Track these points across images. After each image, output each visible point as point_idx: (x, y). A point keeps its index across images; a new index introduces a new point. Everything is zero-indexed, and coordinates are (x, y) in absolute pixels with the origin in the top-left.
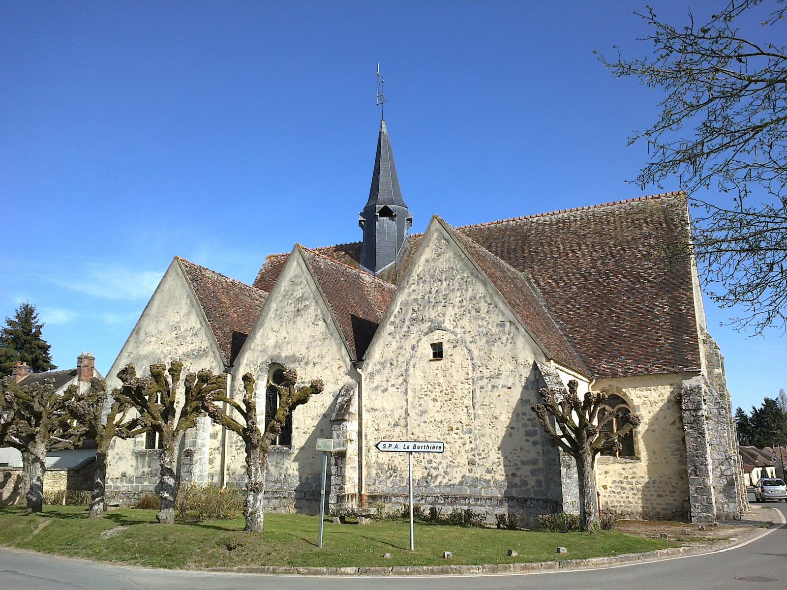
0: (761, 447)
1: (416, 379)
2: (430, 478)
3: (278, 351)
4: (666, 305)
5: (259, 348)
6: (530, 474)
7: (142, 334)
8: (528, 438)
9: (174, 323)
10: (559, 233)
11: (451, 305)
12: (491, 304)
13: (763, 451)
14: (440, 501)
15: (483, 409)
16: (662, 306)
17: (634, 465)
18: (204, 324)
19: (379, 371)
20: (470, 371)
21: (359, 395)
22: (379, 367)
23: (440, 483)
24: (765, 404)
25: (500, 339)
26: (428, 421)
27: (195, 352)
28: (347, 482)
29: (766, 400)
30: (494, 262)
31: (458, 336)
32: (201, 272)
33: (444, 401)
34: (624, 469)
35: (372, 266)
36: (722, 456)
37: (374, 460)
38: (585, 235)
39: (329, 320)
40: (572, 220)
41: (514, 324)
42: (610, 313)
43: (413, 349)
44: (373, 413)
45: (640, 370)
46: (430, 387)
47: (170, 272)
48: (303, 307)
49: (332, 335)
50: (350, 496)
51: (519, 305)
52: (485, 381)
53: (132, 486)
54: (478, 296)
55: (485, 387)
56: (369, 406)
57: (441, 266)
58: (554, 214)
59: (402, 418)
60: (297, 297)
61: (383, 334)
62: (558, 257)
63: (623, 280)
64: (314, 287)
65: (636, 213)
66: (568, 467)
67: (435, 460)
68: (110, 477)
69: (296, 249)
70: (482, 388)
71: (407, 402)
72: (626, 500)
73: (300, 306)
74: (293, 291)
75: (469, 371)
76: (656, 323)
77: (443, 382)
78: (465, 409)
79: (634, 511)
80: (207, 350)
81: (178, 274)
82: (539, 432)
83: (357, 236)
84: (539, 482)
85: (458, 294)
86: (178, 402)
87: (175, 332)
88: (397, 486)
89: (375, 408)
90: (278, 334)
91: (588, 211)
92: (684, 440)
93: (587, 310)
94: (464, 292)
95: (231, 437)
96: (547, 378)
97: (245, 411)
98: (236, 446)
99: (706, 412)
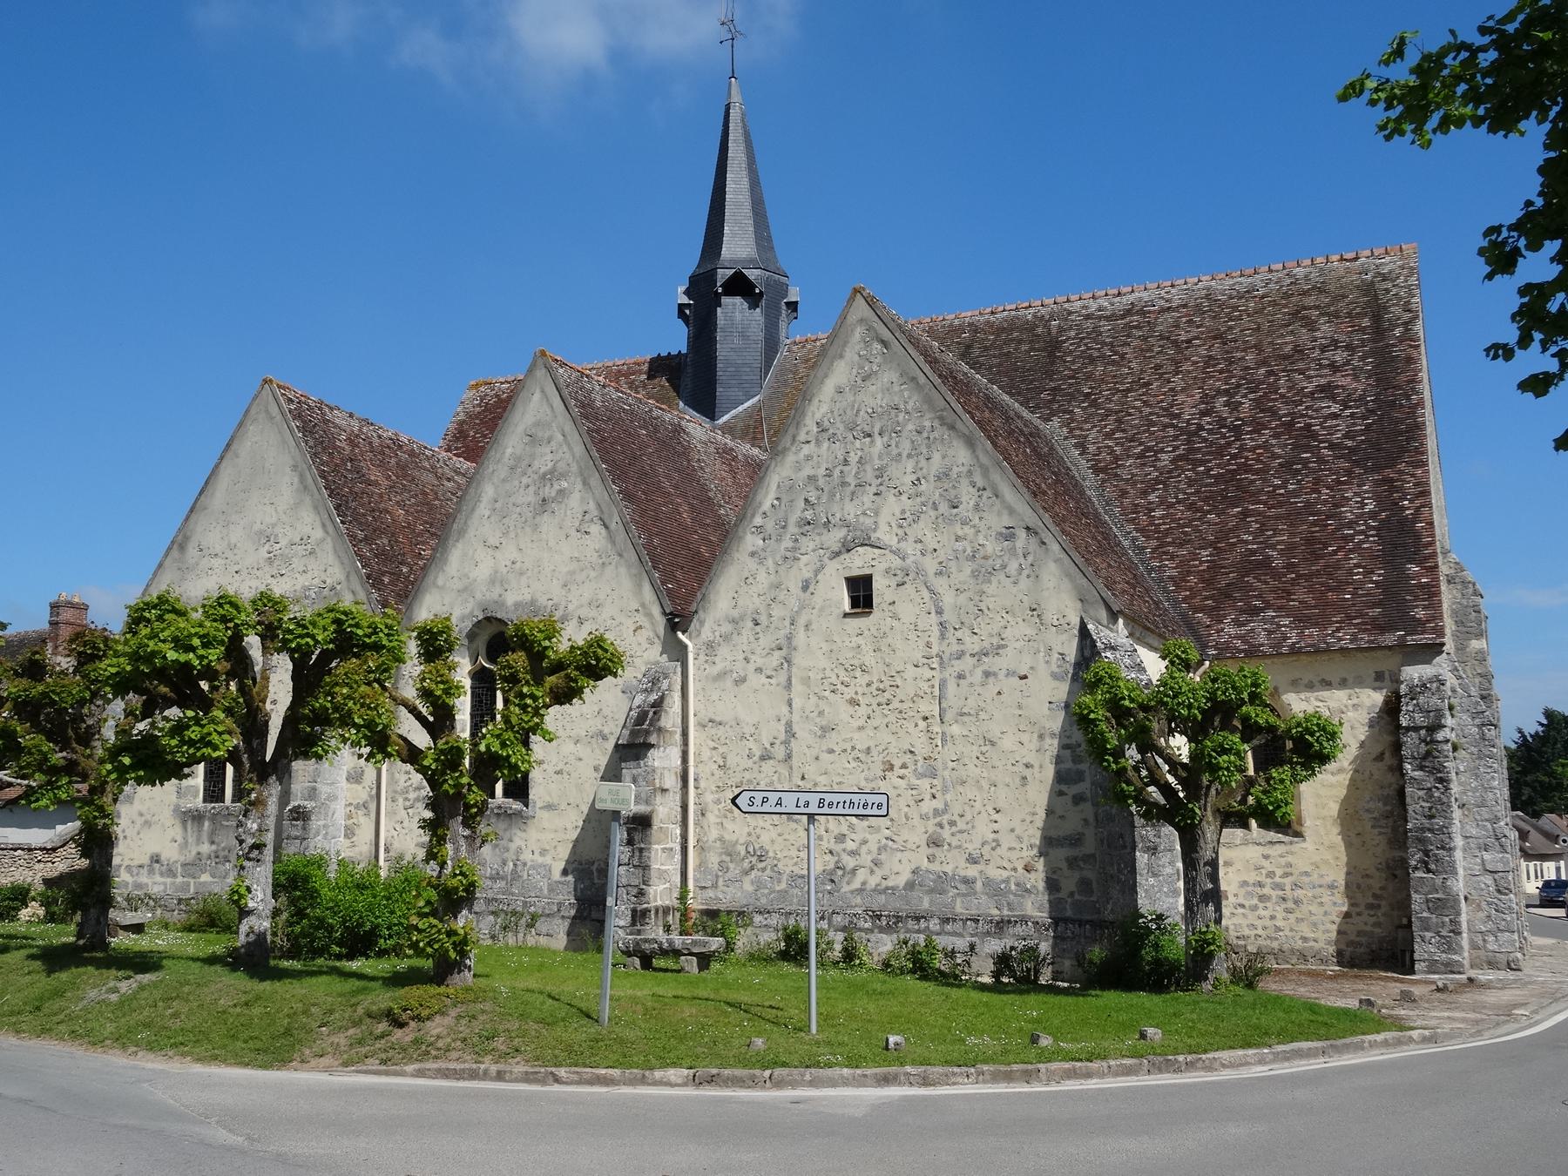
0: (1536, 815)
1: (812, 657)
2: (840, 872)
3: (497, 590)
4: (1368, 498)
5: (457, 585)
6: (1064, 865)
7: (192, 551)
8: (1064, 788)
9: (263, 527)
10: (1130, 337)
11: (893, 491)
12: (984, 489)
13: (1540, 822)
14: (861, 924)
15: (964, 723)
16: (1361, 501)
17: (1288, 847)
18: (330, 529)
19: (726, 638)
20: (934, 640)
21: (682, 689)
22: (727, 628)
23: (864, 883)
24: (1545, 722)
25: (1004, 567)
26: (838, 749)
27: (312, 592)
28: (654, 880)
29: (1549, 714)
30: (988, 397)
31: (909, 561)
32: (324, 414)
33: (875, 706)
34: (1266, 857)
35: (706, 405)
36: (1487, 831)
37: (714, 834)
38: (1189, 341)
39: (615, 521)
40: (1161, 307)
41: (1036, 533)
42: (1245, 514)
43: (805, 588)
44: (713, 731)
45: (1309, 641)
46: (842, 673)
47: (253, 411)
48: (553, 494)
49: (620, 555)
50: (660, 912)
51: (1045, 493)
52: (969, 661)
53: (173, 883)
54: (956, 470)
55: (968, 675)
56: (705, 715)
57: (872, 403)
58: (1119, 294)
59: (778, 742)
60: (542, 471)
61: (736, 555)
62: (1129, 390)
63: (1274, 442)
64: (579, 449)
65: (1305, 293)
66: (1153, 850)
67: (853, 836)
68: (126, 863)
69: (540, 362)
70: (960, 676)
71: (790, 705)
72: (1268, 923)
73: (549, 492)
74: (533, 456)
75: (931, 639)
76: (1347, 539)
77: (873, 662)
78: (922, 724)
79: (1286, 947)
80: (338, 587)
81: (272, 418)
82: (1087, 774)
83: (676, 340)
84: (1085, 885)
85: (910, 465)
86: (274, 702)
87: (267, 547)
88: (766, 891)
89: (718, 719)
90: (498, 554)
91: (1195, 287)
92: (1401, 793)
93: (1191, 507)
94: (923, 463)
95: (392, 780)
96: (1108, 654)
97: (431, 719)
98: (406, 799)
99: (1453, 735)
